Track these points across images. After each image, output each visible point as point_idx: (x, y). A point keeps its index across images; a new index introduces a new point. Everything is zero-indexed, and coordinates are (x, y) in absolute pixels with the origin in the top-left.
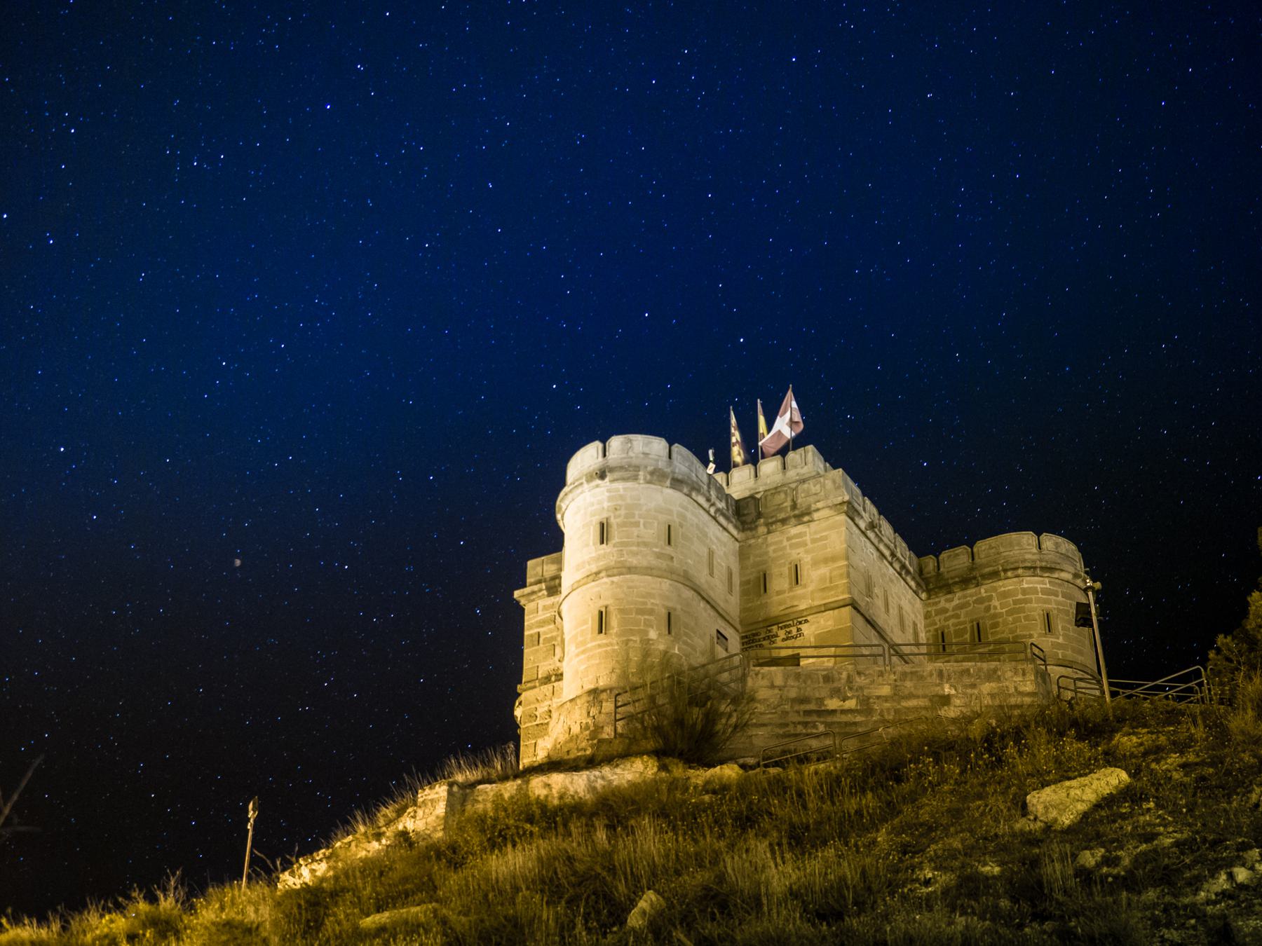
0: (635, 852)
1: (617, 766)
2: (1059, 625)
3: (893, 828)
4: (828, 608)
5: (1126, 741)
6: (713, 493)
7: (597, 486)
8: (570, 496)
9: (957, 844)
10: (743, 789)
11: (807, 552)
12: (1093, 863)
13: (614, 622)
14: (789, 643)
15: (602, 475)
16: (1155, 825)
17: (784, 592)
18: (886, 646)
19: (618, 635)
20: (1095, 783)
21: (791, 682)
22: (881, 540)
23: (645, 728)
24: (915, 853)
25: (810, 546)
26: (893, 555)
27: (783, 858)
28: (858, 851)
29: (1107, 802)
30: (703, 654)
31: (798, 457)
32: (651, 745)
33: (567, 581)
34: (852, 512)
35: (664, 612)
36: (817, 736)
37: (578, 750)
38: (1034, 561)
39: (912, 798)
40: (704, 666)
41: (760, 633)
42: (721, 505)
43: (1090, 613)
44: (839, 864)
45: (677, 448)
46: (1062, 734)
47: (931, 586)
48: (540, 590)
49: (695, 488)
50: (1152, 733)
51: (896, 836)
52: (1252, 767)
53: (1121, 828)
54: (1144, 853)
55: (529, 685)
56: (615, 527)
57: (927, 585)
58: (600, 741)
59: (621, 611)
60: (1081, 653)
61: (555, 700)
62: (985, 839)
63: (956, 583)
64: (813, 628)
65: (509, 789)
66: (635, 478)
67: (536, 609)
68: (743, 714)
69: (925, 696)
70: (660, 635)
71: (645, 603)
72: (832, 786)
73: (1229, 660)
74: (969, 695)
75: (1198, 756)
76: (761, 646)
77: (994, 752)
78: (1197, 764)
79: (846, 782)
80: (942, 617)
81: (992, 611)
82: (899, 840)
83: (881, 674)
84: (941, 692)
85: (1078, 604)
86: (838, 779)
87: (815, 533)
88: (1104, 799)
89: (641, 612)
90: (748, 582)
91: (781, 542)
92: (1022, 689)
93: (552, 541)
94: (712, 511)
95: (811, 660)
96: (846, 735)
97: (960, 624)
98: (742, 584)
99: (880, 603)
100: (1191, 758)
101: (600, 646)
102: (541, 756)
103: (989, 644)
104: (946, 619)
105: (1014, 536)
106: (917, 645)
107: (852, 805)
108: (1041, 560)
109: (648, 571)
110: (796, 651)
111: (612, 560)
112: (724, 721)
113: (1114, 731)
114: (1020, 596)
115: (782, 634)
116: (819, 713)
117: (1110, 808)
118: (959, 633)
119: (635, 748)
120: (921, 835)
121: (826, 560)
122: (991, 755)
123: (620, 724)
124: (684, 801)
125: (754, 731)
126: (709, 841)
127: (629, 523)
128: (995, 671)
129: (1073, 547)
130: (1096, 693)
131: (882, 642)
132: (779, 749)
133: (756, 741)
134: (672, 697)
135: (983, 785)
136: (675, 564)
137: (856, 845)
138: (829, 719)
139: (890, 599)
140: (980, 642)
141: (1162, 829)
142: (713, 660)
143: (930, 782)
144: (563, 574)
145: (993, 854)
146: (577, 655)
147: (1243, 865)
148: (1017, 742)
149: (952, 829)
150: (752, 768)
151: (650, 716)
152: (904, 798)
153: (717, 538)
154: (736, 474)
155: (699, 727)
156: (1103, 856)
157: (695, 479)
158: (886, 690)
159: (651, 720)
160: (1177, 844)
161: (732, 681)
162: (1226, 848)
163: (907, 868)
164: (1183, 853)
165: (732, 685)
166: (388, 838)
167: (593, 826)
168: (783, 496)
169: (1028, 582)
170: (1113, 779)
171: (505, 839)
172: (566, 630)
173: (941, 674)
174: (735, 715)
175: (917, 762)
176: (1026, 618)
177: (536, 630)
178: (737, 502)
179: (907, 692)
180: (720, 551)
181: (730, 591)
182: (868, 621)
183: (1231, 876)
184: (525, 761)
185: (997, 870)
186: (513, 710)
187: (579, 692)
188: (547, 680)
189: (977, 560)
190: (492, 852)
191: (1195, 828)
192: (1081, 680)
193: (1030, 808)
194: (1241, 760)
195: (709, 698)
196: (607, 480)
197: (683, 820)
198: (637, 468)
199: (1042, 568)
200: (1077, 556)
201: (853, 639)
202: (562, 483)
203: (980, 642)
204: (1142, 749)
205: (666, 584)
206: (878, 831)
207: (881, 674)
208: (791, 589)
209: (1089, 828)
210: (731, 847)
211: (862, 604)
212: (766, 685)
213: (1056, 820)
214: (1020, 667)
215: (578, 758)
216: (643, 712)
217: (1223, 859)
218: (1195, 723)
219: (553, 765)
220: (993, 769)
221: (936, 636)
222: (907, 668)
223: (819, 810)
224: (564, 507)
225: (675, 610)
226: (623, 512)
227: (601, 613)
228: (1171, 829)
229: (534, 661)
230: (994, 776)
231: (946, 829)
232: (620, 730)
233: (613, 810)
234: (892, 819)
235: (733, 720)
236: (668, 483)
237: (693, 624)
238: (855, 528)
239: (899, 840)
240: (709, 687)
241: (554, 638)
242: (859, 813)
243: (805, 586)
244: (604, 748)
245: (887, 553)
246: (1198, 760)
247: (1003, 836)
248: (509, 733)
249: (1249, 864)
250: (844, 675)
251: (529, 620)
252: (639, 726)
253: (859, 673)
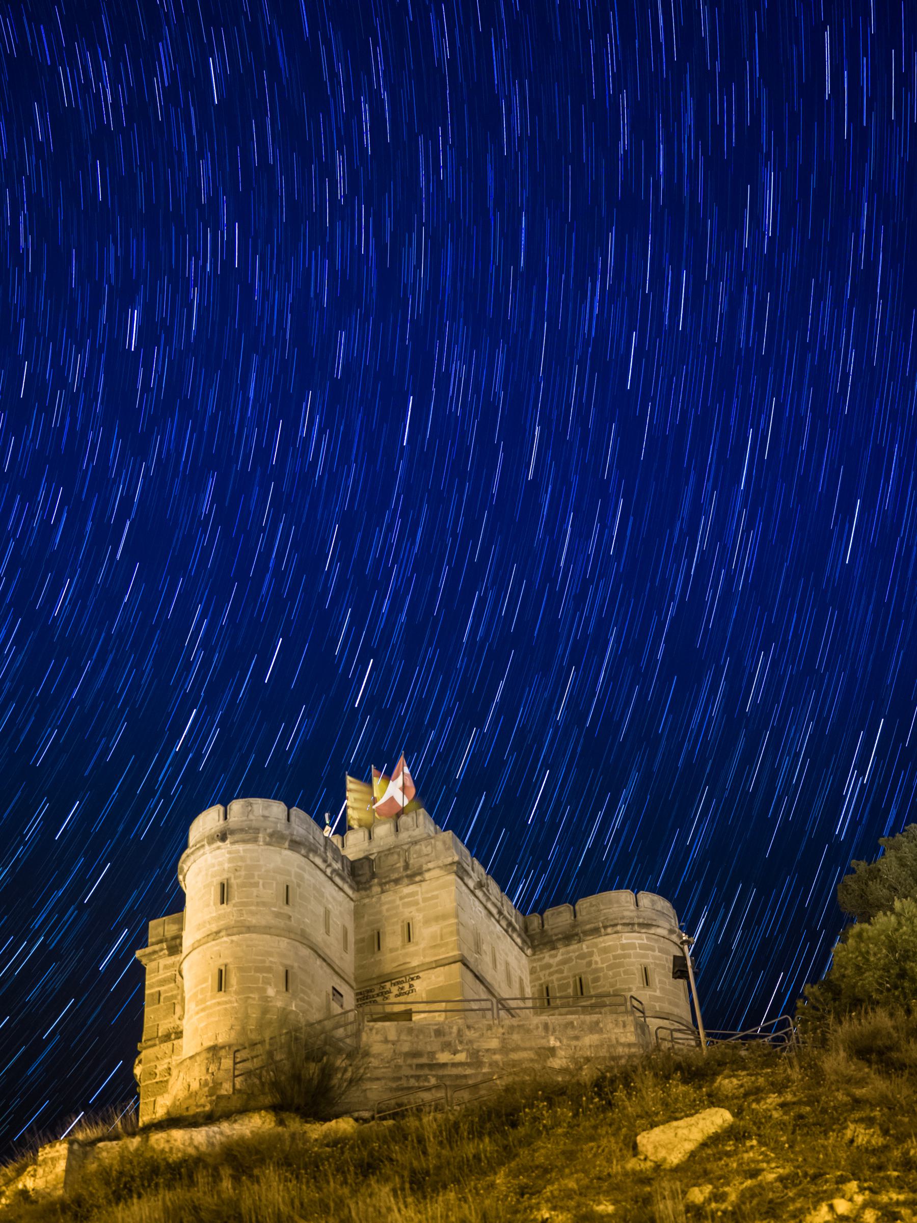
0: (260, 1200)
1: (235, 1121)
2: (656, 979)
3: (510, 1171)
4: (439, 964)
5: (727, 1084)
6: (329, 855)
7: (219, 848)
8: (192, 858)
9: (572, 1184)
10: (363, 1140)
11: (419, 910)
12: (702, 1199)
13: (233, 980)
14: (402, 999)
15: (223, 837)
16: (758, 1162)
17: (397, 949)
18: (494, 1000)
19: (237, 993)
20: (701, 1122)
21: (404, 1037)
22: (489, 899)
23: (263, 1084)
24: (532, 1194)
25: (422, 905)
26: (500, 913)
27: (405, 1202)
28: (478, 1194)
29: (714, 1140)
32: (268, 1100)
33: (188, 941)
34: (461, 872)
35: (282, 970)
36: (429, 1089)
37: (197, 1106)
38: (631, 918)
39: (527, 1141)
40: (320, 1022)
41: (373, 990)
42: (337, 866)
43: (686, 965)
44: (460, 1207)
45: (295, 811)
46: (667, 1077)
47: (536, 943)
48: (162, 950)
49: (313, 849)
50: (751, 1075)
51: (514, 1178)
52: (846, 1105)
53: (727, 1165)
54: (750, 1189)
55: (149, 1043)
56: (235, 887)
57: (532, 942)
58: (220, 1097)
59: (241, 969)
60: (677, 1005)
61: (174, 1057)
62: (599, 1179)
63: (559, 940)
64: (425, 984)
65: (135, 1142)
66: (255, 840)
67: (157, 969)
68: (358, 1068)
69: (531, 1049)
70: (277, 992)
71: (264, 961)
73: (816, 1008)
74: (572, 1045)
75: (795, 1095)
76: (375, 1002)
77: (604, 1096)
78: (794, 1103)
79: (464, 1128)
80: (547, 972)
81: (594, 966)
82: (517, 1182)
83: (490, 1028)
84: (546, 1045)
85: (675, 957)
86: (456, 1126)
87: (427, 892)
88: (710, 1138)
89: (258, 970)
90: (363, 940)
91: (394, 901)
93: (175, 902)
94: (329, 871)
95: (423, 1015)
96: (457, 1088)
97: (564, 978)
98: (355, 943)
99: (488, 959)
100: (789, 1097)
101: (219, 1004)
102: (161, 1113)
103: (592, 997)
104: (551, 974)
105: (613, 894)
106: (524, 999)
107: (470, 1149)
109: (266, 930)
110: (409, 1007)
111: (231, 920)
112: (339, 1076)
113: (715, 1074)
114: (619, 952)
115: (395, 990)
116: (431, 1066)
117: (717, 1146)
118: (563, 987)
119: (252, 1103)
120: (538, 1177)
121: (437, 918)
122: (601, 1099)
123: (238, 1081)
125: (368, 1085)
128: (597, 1023)
129: (667, 904)
130: (692, 1044)
131: (490, 997)
132: (393, 1102)
133: (370, 1095)
134: (290, 1053)
135: (595, 1127)
136: (293, 923)
137: (476, 1188)
138: (441, 1072)
142: (329, 1016)
143: (544, 1126)
144: (184, 934)
145: (607, 1193)
146: (197, 1013)
147: (843, 1197)
148: (627, 1085)
150: (366, 1121)
151: (268, 1072)
152: (520, 1142)
153: (334, 898)
154: (351, 837)
155: (315, 1082)
156: (711, 1193)
157: (312, 840)
158: (494, 1044)
160: (781, 1179)
161: (347, 1036)
162: (826, 1181)
163: (525, 1209)
164: (786, 1187)
165: (348, 1041)
166: (7, 1197)
167: (219, 1174)
168: (396, 857)
169: (628, 938)
170: (717, 1119)
171: (130, 1191)
173: (546, 1027)
174: (350, 1069)
175: (531, 1106)
176: (625, 972)
177: (157, 989)
178: (352, 863)
179: (513, 1046)
181: (346, 949)
182: (476, 976)
183: (831, 1208)
184: (145, 1119)
185: (611, 1208)
186: (132, 1068)
187: (198, 1050)
188: (167, 1038)
189: (579, 918)
190: (117, 1204)
191: (796, 1164)
192: (679, 1031)
193: (640, 1148)
194: (835, 1098)
195: (325, 1053)
196: (228, 842)
197: (306, 1169)
198: (257, 830)
199: (639, 924)
200: (672, 912)
201: (463, 995)
202: (186, 846)
203: (583, 995)
204: (742, 1090)
205: (284, 943)
206: (496, 1174)
207: (490, 1028)
208: (403, 946)
209: (696, 1166)
211: (471, 961)
212: (381, 1039)
213: (665, 1159)
214: (621, 1019)
215: (195, 1116)
216: (262, 1067)
217: (825, 1192)
218: (792, 1067)
219: (172, 1121)
220: (603, 1112)
221: (541, 991)
222: (515, 1022)
223: (439, 1156)
224: (186, 868)
225: (292, 967)
226: (243, 873)
227: (221, 971)
228: (773, 1165)
229: (154, 1019)
231: (561, 1170)
232: (238, 1086)
233: (240, 1160)
234: (509, 1162)
235: (349, 1075)
236: (286, 845)
238: (464, 888)
242: (477, 1157)
243: (417, 944)
244: (223, 1104)
245: (494, 911)
246: (795, 1099)
247: (616, 1176)
249: (848, 1196)
250: (455, 1030)
251: (150, 980)
252: (257, 1081)
253: (469, 1027)
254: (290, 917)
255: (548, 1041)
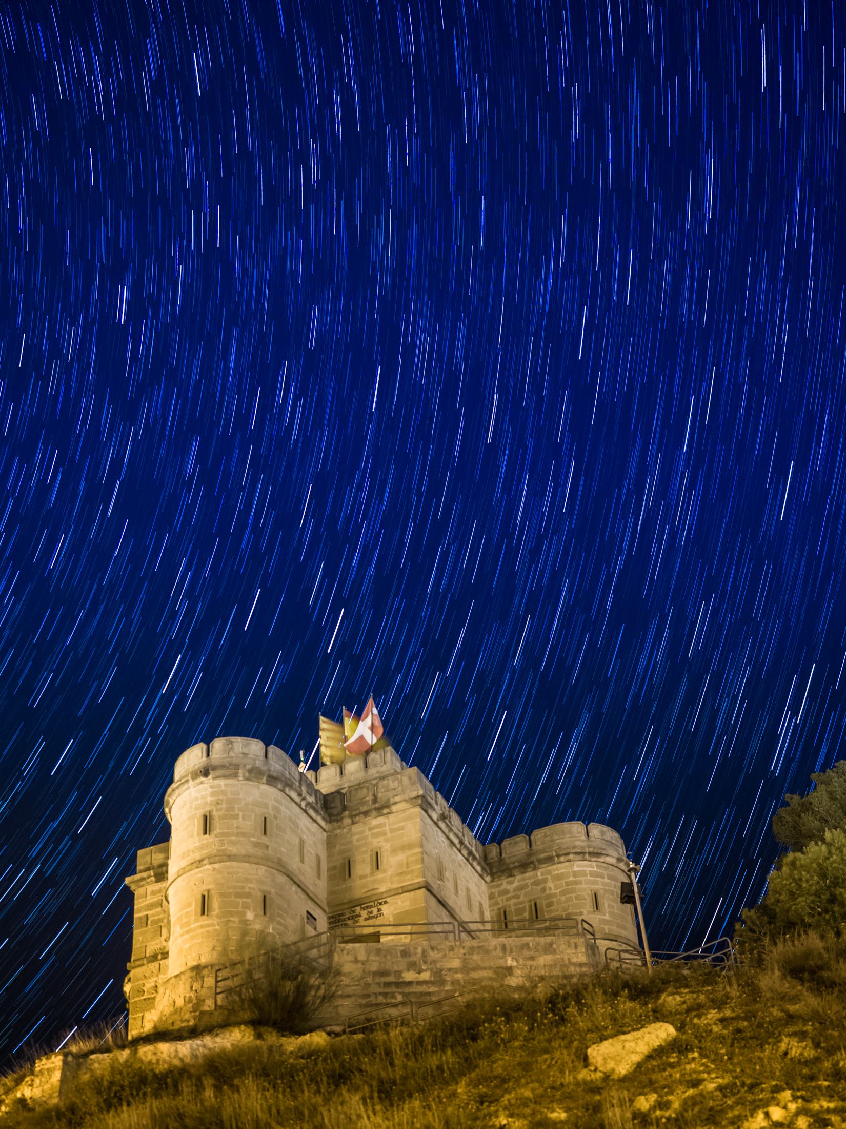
0: (240, 1108)
1: (217, 1035)
2: (605, 903)
3: (471, 1081)
4: (405, 890)
5: (671, 1000)
6: (304, 789)
7: (202, 783)
8: (177, 792)
9: (527, 1093)
10: (336, 1052)
11: (386, 840)
12: (647, 1107)
13: (215, 904)
14: (371, 922)
15: (205, 773)
16: (700, 1072)
18: (456, 924)
19: (218, 917)
20: (647, 1036)
21: (372, 957)
22: (451, 830)
23: (242, 1001)
24: (491, 1102)
25: (389, 835)
26: (461, 843)
27: (374, 1110)
28: (441, 1102)
29: (658, 1053)
30: (294, 933)
31: (378, 756)
32: (247, 1015)
33: (173, 870)
34: (425, 805)
35: (260, 895)
36: (395, 1006)
37: (182, 1021)
38: (583, 847)
39: (486, 1054)
40: (295, 943)
41: (345, 914)
42: (311, 799)
43: (633, 891)
44: (424, 1114)
45: (272, 748)
46: (616, 995)
47: (495, 870)
48: (149, 877)
49: (288, 784)
50: (693, 993)
52: (780, 1020)
53: (671, 1076)
54: (692, 1097)
55: (138, 963)
56: (217, 819)
57: (491, 869)
58: (203, 1013)
59: (222, 895)
60: (624, 928)
61: (161, 976)
62: (553, 1088)
63: (516, 867)
64: (392, 908)
66: (235, 775)
68: (331, 986)
69: (490, 968)
70: (256, 916)
71: (243, 888)
72: (416, 1046)
74: (528, 964)
75: (733, 1011)
77: (557, 1012)
78: (733, 1018)
79: (428, 1041)
80: (505, 897)
82: (476, 1091)
83: (452, 949)
84: (504, 965)
85: (622, 883)
86: (421, 1039)
88: (655, 1050)
89: (238, 895)
90: (334, 868)
91: (363, 832)
92: (574, 960)
93: (163, 833)
94: (303, 804)
95: (390, 937)
96: (422, 1004)
97: (521, 903)
98: (329, 870)
99: (450, 885)
100: (728, 1013)
101: (202, 926)
102: (148, 1027)
103: (545, 920)
104: (508, 899)
105: (566, 825)
106: (483, 922)
107: (433, 1061)
108: (589, 847)
109: (246, 858)
110: (377, 929)
111: (214, 849)
112: (313, 993)
113: (660, 992)
114: (571, 879)
115: (364, 914)
116: (398, 984)
117: (661, 1058)
118: (519, 911)
119: (233, 1019)
120: (496, 1087)
121: (403, 848)
122: (555, 1015)
123: (220, 997)
124: (283, 1062)
125: (339, 1002)
126: (307, 1095)
127: (230, 815)
128: (551, 944)
130: (638, 964)
131: (452, 920)
132: (363, 1017)
134: (267, 972)
135: (549, 1041)
137: (439, 1097)
138: (407, 990)
139: (459, 882)
140: (537, 919)
141: (706, 1075)
142: (304, 938)
143: (502, 1039)
144: (170, 862)
145: (560, 1101)
146: (182, 935)
147: (778, 1105)
148: (578, 1002)
149: (523, 1081)
150: (337, 1035)
151: (247, 989)
152: (480, 1054)
153: (308, 829)
154: (324, 773)
155: (291, 999)
156: (656, 1101)
157: (288, 776)
158: (456, 963)
159: (248, 993)
160: (720, 1088)
161: (321, 957)
162: (763, 1090)
164: (725, 1096)
165: (321, 961)
166: (7, 1105)
167: (202, 1084)
168: (365, 791)
169: (579, 866)
171: (120, 1099)
172: (171, 913)
173: (504, 948)
174: (323, 987)
175: (490, 1021)
177: (145, 913)
178: (325, 796)
180: (309, 840)
182: (439, 901)
183: (767, 1115)
184: (133, 1033)
185: (563, 1116)
186: (122, 986)
187: (183, 969)
188: (154, 958)
189: (534, 847)
190: (108, 1111)
191: (734, 1074)
192: (627, 951)
193: (591, 1060)
194: (771, 1014)
195: (300, 972)
196: (210, 777)
198: (237, 766)
199: (590, 853)
200: (619, 842)
201: (427, 918)
202: (171, 781)
203: (537, 919)
204: (685, 1006)
205: (262, 871)
206: (457, 1083)
208: (372, 874)
209: (643, 1076)
210: (327, 1101)
211: (435, 887)
212: (351, 959)
213: (613, 1070)
214: (573, 940)
215: (179, 1030)
216: (241, 986)
217: (761, 1100)
218: (730, 985)
219: (159, 1035)
220: (557, 1026)
221: (499, 915)
222: (475, 943)
223: (405, 1067)
224: (171, 801)
225: (270, 893)
226: (224, 806)
227: (204, 896)
228: (713, 1075)
229: (143, 941)
230: (558, 1032)
231: (518, 1080)
232: (219, 1003)
233: (222, 1071)
234: (470, 1073)
235: (322, 992)
236: (264, 780)
237: (286, 906)
238: (428, 819)
239: (476, 1091)
240: (300, 962)
241: (160, 920)
242: (440, 1068)
243: (385, 871)
244: (205, 1019)
245: (456, 841)
246: (734, 1015)
247: (568, 1086)
248: (118, 1006)
249: (782, 1104)
250: (419, 951)
251: (138, 904)
252: (237, 998)
253: (432, 948)
254: (267, 847)
255: (506, 961)
